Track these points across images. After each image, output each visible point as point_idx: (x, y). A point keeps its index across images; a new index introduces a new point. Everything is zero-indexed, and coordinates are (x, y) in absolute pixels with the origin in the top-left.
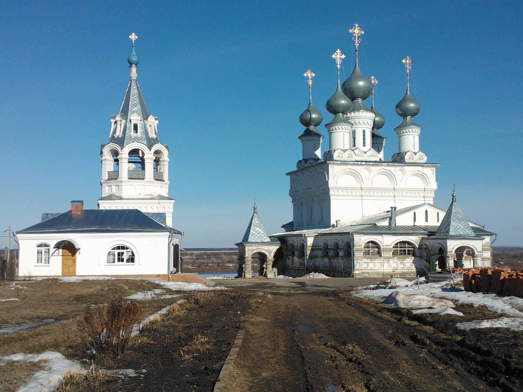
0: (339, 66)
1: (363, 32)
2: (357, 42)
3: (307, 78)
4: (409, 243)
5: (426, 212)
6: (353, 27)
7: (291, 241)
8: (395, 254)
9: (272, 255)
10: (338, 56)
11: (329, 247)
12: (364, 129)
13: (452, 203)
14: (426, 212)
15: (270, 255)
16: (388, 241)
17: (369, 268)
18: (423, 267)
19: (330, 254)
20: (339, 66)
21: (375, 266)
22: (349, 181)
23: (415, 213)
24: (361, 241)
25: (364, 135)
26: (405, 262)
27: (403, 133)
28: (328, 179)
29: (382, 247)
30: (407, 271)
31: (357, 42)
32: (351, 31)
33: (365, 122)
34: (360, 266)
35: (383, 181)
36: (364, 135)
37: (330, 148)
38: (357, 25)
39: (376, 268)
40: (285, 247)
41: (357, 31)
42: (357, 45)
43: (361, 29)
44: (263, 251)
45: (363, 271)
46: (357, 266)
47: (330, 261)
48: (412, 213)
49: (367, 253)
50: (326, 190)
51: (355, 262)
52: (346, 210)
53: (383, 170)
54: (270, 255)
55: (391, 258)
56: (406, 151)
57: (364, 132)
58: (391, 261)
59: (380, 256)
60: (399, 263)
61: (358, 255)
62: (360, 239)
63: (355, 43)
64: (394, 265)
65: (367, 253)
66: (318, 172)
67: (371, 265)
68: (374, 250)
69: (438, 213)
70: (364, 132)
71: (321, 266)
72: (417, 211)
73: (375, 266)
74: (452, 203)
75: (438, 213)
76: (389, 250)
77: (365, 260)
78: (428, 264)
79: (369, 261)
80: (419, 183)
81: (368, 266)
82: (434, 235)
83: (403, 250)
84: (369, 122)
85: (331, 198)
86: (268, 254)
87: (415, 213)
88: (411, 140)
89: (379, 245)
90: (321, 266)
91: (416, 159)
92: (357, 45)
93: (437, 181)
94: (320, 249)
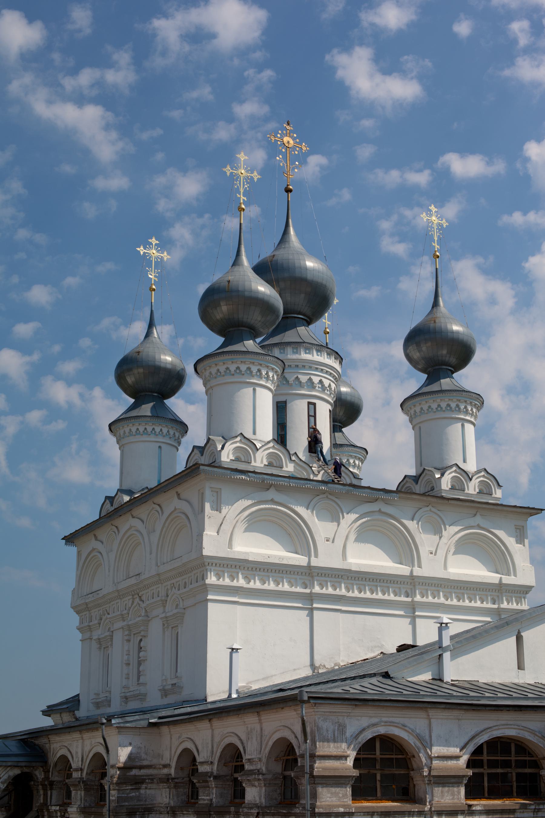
7: (63, 752)
11: (202, 769)
19: (204, 798)
40: (39, 775)
66: (167, 512)
94: (167, 779)
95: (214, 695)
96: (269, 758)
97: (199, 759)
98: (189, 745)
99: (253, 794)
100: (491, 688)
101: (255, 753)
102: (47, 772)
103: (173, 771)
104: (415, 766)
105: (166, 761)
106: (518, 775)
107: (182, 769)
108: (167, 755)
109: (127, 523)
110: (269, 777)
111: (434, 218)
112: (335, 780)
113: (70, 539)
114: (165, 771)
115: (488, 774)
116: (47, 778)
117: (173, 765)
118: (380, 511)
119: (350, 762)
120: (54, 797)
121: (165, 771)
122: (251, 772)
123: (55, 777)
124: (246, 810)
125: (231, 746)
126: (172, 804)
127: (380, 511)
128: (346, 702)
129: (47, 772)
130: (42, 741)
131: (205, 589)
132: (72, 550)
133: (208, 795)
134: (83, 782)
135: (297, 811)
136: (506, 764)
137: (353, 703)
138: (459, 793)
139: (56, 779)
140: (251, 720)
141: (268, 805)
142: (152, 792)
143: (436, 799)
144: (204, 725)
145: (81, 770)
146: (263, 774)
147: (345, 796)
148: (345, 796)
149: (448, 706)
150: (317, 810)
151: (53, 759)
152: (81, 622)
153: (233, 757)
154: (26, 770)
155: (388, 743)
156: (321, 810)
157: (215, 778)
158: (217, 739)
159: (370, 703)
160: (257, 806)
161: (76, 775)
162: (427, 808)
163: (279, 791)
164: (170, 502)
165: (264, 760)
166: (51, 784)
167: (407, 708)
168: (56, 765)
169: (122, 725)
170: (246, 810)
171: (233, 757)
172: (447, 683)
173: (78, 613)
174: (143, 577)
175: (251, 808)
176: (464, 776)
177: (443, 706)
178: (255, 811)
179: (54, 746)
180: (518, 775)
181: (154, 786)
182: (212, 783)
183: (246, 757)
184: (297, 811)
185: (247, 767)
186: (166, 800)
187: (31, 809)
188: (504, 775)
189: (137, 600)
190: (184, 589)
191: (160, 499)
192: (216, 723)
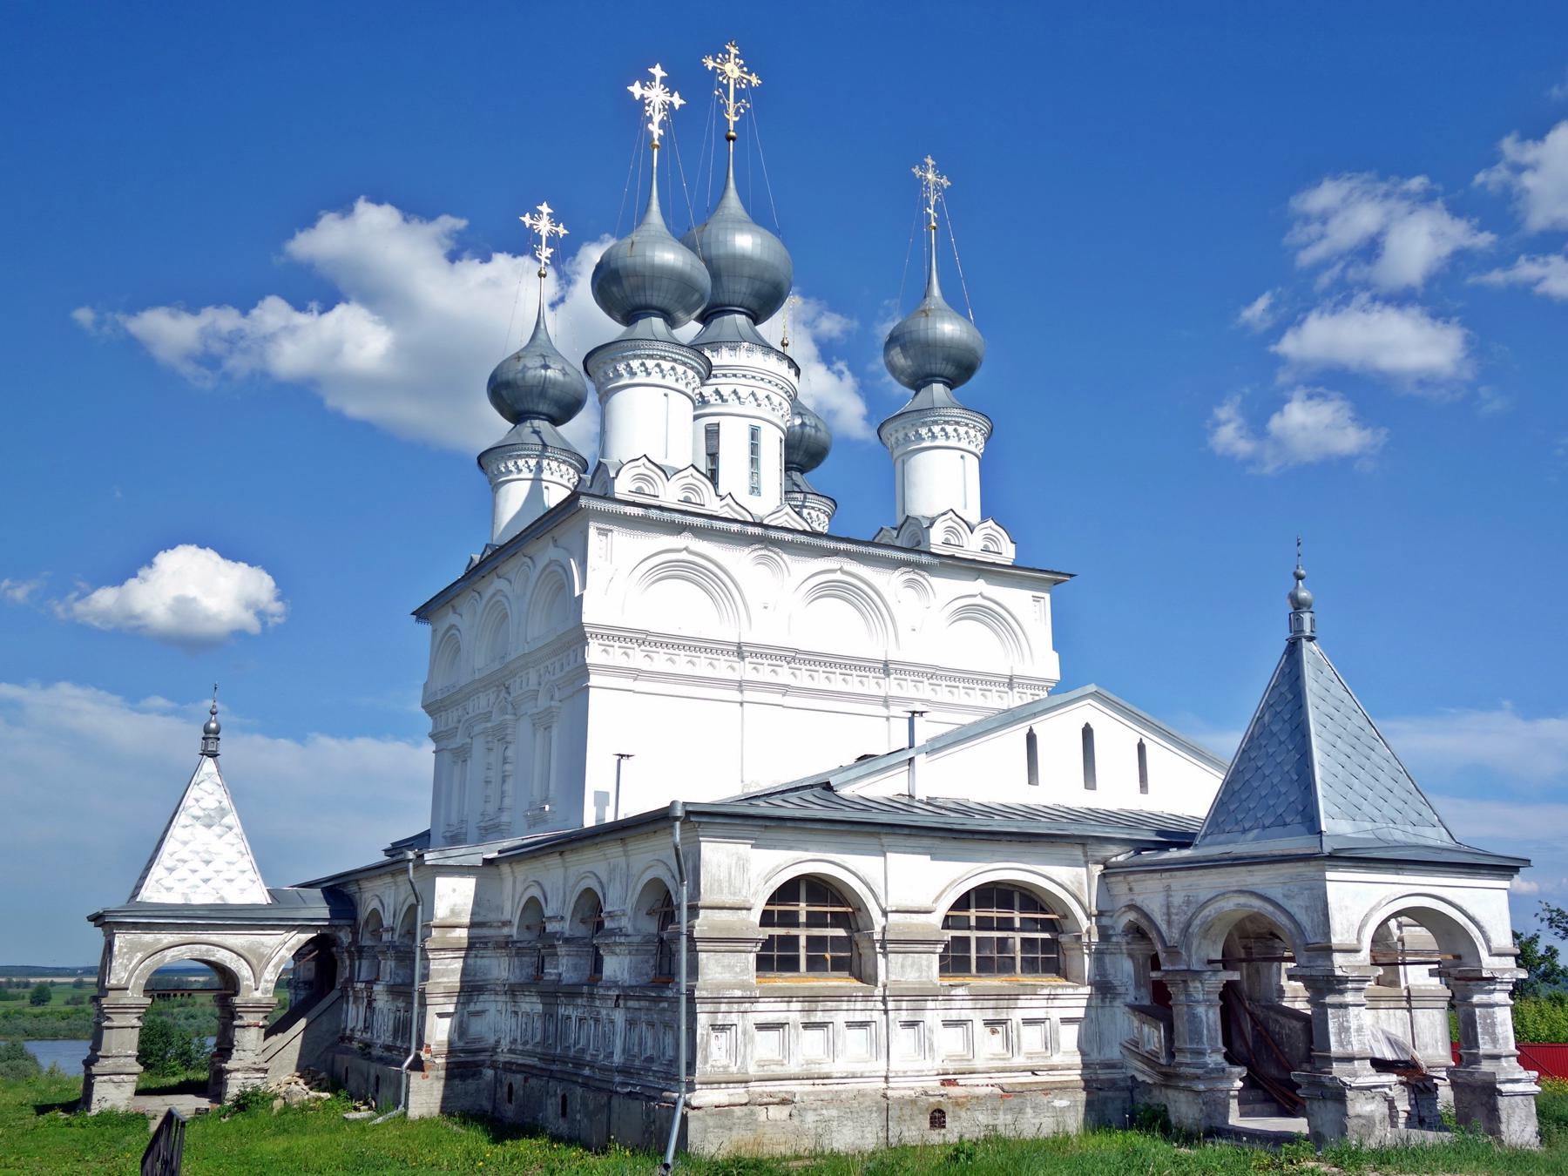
0: (655, 130)
1: (755, 81)
2: (731, 110)
3: (535, 213)
4: (1030, 898)
5: (1087, 733)
6: (718, 50)
7: (375, 904)
8: (954, 961)
9: (270, 976)
10: (656, 96)
11: (551, 927)
12: (756, 423)
13: (1293, 649)
14: (1087, 733)
15: (257, 977)
16: (910, 888)
17: (793, 1068)
18: (1114, 1053)
20: (655, 130)
21: (832, 1048)
22: (681, 608)
23: (1031, 739)
24: (740, 878)
25: (754, 449)
26: (1016, 1016)
27: (920, 438)
28: (584, 586)
29: (878, 921)
30: (1027, 1078)
31: (731, 110)
32: (710, 64)
33: (761, 394)
34: (733, 1052)
35: (836, 628)
36: (754, 449)
37: (603, 454)
38: (734, 51)
39: (838, 1067)
40: (345, 937)
41: (732, 70)
42: (733, 118)
43: (750, 64)
44: (221, 956)
45: (756, 1088)
46: (715, 1053)
47: (548, 1015)
48: (1018, 734)
49: (777, 957)
50: (574, 638)
51: (703, 1020)
52: (645, 748)
53: (838, 576)
54: (257, 977)
55: (935, 996)
56: (930, 513)
57: (754, 433)
58: (933, 1016)
59: (866, 976)
60: (978, 1026)
61: (723, 971)
62: (743, 866)
63: (724, 107)
64: (949, 1043)
65: (775, 958)
66: (541, 564)
67: (809, 1048)
68: (818, 933)
69: (1141, 748)
70: (754, 433)
71: (505, 1045)
72: (1041, 727)
73: (832, 1048)
74: (1293, 649)
75: (1141, 748)
76: (911, 943)
77: (769, 1011)
78: (1153, 1037)
79: (793, 1014)
80: (976, 648)
81: (785, 1048)
82: (1187, 846)
83: (1001, 934)
84: (776, 400)
85: (594, 680)
86: (243, 971)
87: (1031, 739)
88: (945, 478)
89: (860, 908)
90: (505, 1045)
91: (972, 546)
92: (733, 118)
93: (1056, 647)
94: (506, 944)
95: (1524, 1094)
96: (637, 909)
97: (548, 912)
98: (535, 892)
99: (615, 966)
100: (988, 811)
101: (621, 903)
102: (355, 933)
103: (514, 931)
104: (861, 925)
105: (507, 916)
106: (1023, 940)
107: (528, 928)
108: (508, 906)
109: (494, 585)
110: (637, 939)
111: (930, 176)
112: (730, 942)
113: (423, 614)
114: (506, 931)
115: (978, 939)
116: (354, 942)
117: (516, 922)
118: (841, 569)
119: (755, 916)
120: (364, 969)
121: (506, 931)
122: (612, 932)
123: (367, 941)
124: (602, 991)
125: (588, 891)
126: (513, 980)
127: (841, 569)
128: (750, 822)
129: (355, 933)
130: (353, 888)
131: (583, 671)
132: (425, 629)
133: (556, 967)
134: (394, 947)
135: (669, 994)
136: (1006, 925)
137: (761, 822)
138: (929, 967)
139: (369, 943)
140: (614, 851)
141: (634, 983)
142: (486, 962)
143: (893, 977)
144: (554, 861)
145: (393, 929)
146: (627, 936)
147: (745, 970)
148: (745, 970)
149: (914, 831)
150: (697, 994)
151: (363, 914)
152: (435, 727)
153: (591, 906)
154: (326, 931)
155: (818, 888)
156: (704, 994)
157: (567, 941)
158: (571, 882)
159: (789, 824)
160: (615, 984)
161: (386, 937)
162: (879, 991)
163: (652, 962)
164: (546, 552)
165: (629, 912)
166: (360, 950)
167: (849, 833)
168: (367, 922)
169: (440, 862)
170: (602, 991)
171: (591, 906)
172: (920, 801)
173: (430, 713)
174: (508, 659)
175: (609, 988)
176: (937, 942)
177: (906, 831)
178: (614, 993)
179: (367, 895)
180: (1023, 940)
181: (489, 953)
182: (562, 950)
183: (607, 908)
184: (669, 994)
185: (607, 925)
186: (505, 974)
187: (332, 987)
188: (1003, 942)
189: (503, 694)
190: (559, 671)
191: (533, 548)
192: (571, 858)
